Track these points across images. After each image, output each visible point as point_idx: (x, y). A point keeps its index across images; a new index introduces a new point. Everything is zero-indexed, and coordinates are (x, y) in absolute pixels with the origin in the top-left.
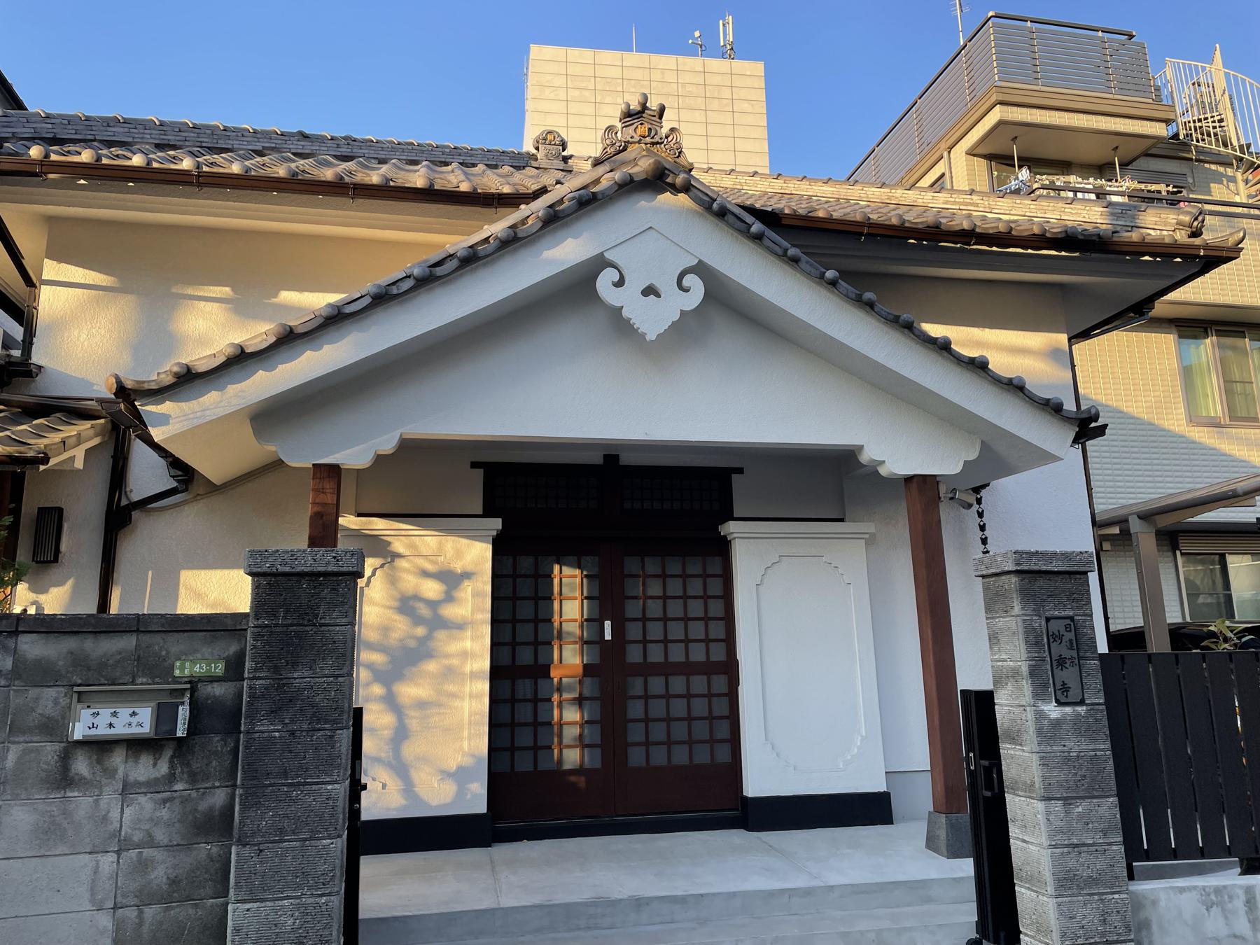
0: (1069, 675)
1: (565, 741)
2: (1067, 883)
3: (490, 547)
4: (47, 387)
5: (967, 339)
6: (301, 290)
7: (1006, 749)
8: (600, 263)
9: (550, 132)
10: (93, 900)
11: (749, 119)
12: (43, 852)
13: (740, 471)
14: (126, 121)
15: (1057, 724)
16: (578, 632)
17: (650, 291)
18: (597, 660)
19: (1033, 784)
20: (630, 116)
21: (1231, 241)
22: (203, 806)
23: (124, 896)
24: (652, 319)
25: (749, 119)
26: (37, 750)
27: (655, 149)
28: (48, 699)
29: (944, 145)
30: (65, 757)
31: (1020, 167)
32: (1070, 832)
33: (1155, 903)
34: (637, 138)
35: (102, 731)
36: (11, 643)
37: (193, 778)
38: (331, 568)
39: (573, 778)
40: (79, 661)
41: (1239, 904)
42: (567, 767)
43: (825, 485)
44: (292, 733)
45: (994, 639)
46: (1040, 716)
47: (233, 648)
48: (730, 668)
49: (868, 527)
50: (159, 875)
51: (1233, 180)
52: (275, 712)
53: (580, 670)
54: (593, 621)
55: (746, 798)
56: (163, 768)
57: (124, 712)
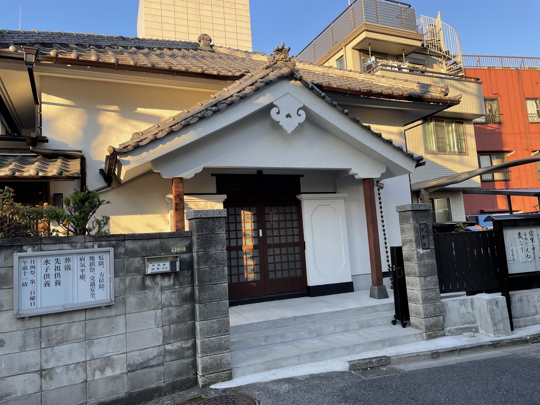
0: (425, 241)
1: (249, 271)
2: (425, 300)
3: (222, 205)
4: (51, 146)
5: (375, 128)
6: (145, 107)
7: (406, 263)
8: (271, 106)
9: (205, 35)
10: (156, 325)
11: (243, 13)
12: (140, 310)
13: (302, 176)
14: (66, 34)
15: (422, 255)
16: (251, 234)
17: (288, 116)
18: (257, 244)
19: (416, 273)
20: (278, 50)
21: (457, 98)
22: (184, 293)
23: (165, 322)
24: (289, 125)
25: (243, 13)
26: (134, 278)
27: (286, 63)
28: (136, 262)
29: (343, 44)
30: (143, 280)
31: (372, 55)
32: (426, 286)
33: (447, 305)
34: (280, 59)
35: (156, 271)
36: (123, 243)
37: (181, 284)
38: (218, 216)
39: (252, 284)
40: (144, 248)
41: (469, 303)
42: (249, 280)
43: (333, 181)
44: (211, 268)
45: (402, 231)
46: (418, 253)
47: (188, 242)
48: (302, 245)
49: (345, 195)
50: (174, 315)
51: (442, 63)
52: (206, 262)
53: (252, 247)
54: (256, 230)
55: (309, 287)
56: (172, 282)
57: (161, 264)
